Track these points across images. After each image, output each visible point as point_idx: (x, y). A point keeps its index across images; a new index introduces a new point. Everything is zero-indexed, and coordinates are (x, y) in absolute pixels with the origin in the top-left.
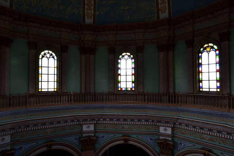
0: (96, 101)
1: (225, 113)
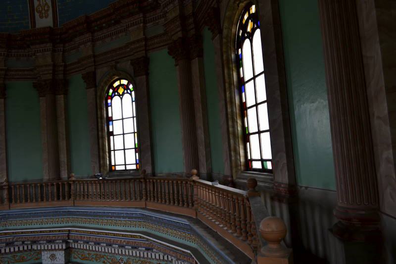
0: (61, 198)
1: (4, 211)
